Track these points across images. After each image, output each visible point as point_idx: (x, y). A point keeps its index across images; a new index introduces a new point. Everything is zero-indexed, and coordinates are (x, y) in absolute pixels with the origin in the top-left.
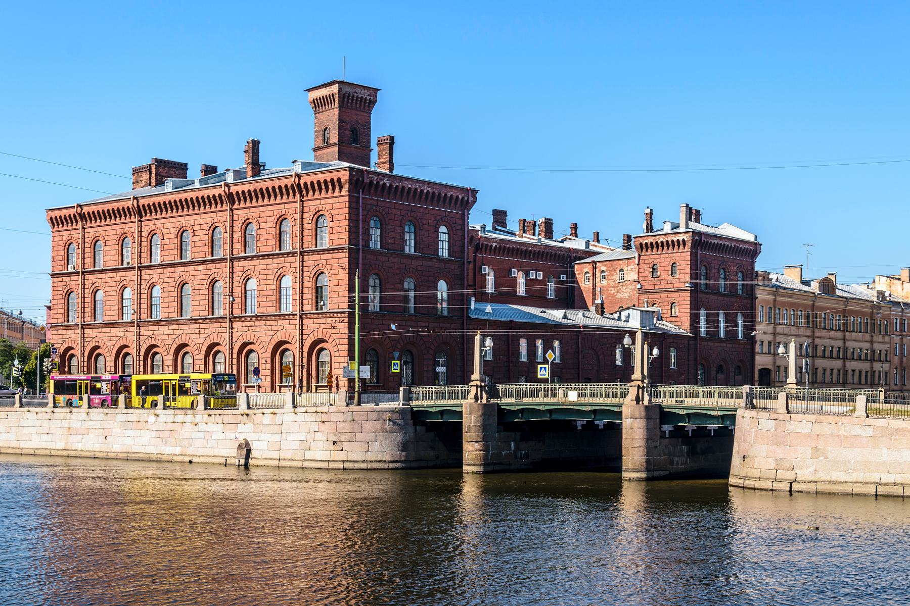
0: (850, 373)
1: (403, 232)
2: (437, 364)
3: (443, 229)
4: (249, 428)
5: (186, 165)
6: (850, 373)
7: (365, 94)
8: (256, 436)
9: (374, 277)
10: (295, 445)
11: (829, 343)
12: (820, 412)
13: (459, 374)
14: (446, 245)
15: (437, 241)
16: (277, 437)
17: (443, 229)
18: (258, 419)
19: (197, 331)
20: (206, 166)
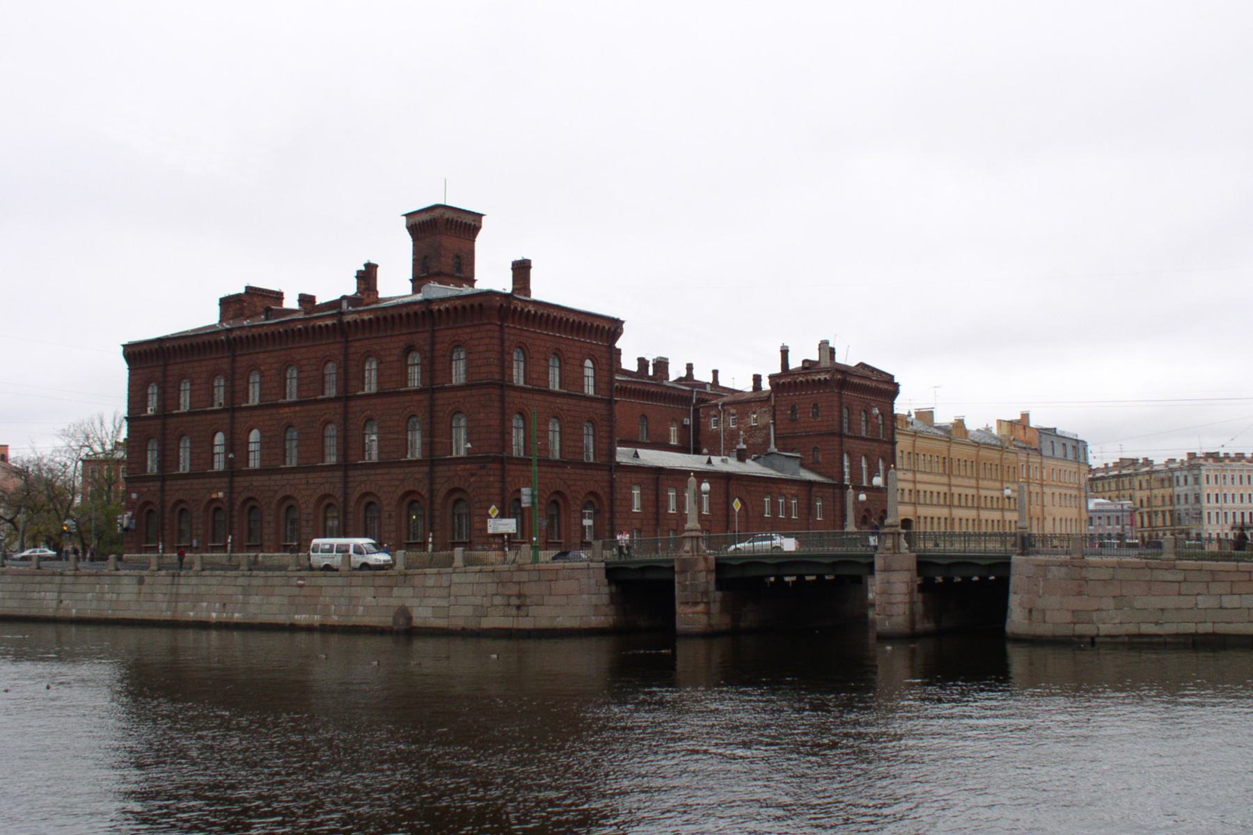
0: (957, 521)
1: (548, 367)
2: (583, 516)
3: (588, 363)
4: (409, 591)
5: (281, 294)
6: (957, 521)
7: (468, 220)
8: (416, 602)
9: (518, 416)
10: (469, 611)
11: (964, 491)
12: (254, 565)
13: (607, 527)
14: (591, 381)
15: (582, 376)
16: (444, 603)
17: (588, 363)
18: (417, 581)
19: (304, 481)
20: (376, 266)
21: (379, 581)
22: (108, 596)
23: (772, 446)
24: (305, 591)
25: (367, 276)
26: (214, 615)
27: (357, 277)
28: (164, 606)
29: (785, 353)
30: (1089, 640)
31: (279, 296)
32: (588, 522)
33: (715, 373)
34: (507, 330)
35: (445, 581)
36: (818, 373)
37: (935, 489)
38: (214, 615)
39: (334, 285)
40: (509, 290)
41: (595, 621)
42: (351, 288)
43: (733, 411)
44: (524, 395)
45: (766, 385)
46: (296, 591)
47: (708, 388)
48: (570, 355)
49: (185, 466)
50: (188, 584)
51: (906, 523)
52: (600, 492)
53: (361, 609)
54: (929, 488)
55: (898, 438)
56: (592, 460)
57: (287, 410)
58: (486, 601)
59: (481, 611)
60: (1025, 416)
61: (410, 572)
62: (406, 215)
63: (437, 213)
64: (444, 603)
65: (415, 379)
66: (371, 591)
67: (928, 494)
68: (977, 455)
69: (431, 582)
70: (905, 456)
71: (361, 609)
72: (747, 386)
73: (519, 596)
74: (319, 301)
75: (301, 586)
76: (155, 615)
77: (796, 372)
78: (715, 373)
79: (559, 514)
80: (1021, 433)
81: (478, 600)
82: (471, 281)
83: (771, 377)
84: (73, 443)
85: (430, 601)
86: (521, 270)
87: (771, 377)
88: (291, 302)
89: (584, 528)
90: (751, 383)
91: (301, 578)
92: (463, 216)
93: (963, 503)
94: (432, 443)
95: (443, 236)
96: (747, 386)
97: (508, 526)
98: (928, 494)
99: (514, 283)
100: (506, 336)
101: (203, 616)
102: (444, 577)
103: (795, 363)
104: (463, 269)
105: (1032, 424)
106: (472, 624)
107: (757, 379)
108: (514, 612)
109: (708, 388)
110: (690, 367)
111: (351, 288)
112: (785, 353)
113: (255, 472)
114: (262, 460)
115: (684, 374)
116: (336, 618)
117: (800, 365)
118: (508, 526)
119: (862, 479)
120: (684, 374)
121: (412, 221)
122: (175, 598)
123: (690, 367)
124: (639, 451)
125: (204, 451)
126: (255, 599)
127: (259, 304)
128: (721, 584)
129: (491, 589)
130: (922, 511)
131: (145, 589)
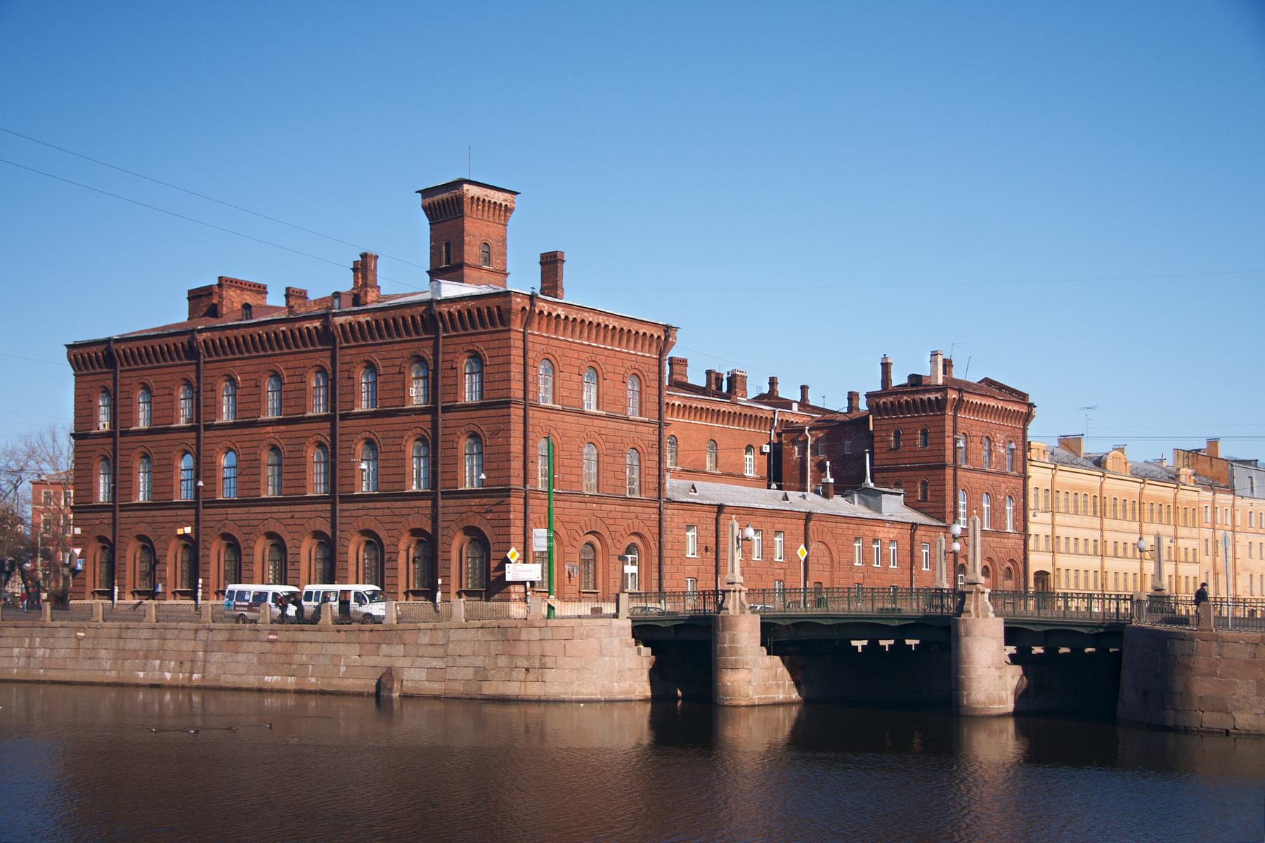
8: (406, 662)
16: (439, 664)
18: (408, 637)
21: (366, 637)
22: (40, 652)
23: (869, 480)
24: (278, 647)
25: (364, 267)
26: (168, 676)
28: (108, 665)
29: (886, 367)
31: (261, 290)
32: (630, 569)
33: (804, 389)
34: (530, 338)
35: (440, 637)
36: (929, 391)
37: (1082, 534)
39: (327, 280)
42: (346, 283)
44: (552, 416)
45: (863, 405)
46: (268, 646)
47: (795, 407)
48: (610, 368)
49: (102, 496)
50: (139, 639)
51: (1042, 576)
52: (645, 532)
53: (343, 669)
54: (1072, 533)
55: (1031, 471)
57: (269, 429)
58: (488, 662)
60: (1213, 443)
61: (401, 626)
62: (68, 346)
64: (439, 664)
65: (416, 394)
66: (356, 648)
67: (1072, 542)
68: (1175, 498)
69: (425, 639)
70: (1041, 493)
71: (343, 669)
72: (841, 405)
74: (313, 296)
76: (97, 677)
77: (901, 389)
78: (804, 389)
79: (595, 560)
80: (1207, 467)
81: (479, 661)
83: (868, 395)
84: (11, 464)
85: (424, 662)
86: (551, 264)
87: (868, 395)
88: (275, 299)
89: (624, 577)
91: (273, 632)
93: (1081, 550)
94: (114, 488)
96: (841, 405)
97: (533, 572)
98: (1072, 542)
99: (543, 281)
100: (530, 345)
101: (154, 677)
102: (441, 633)
105: (1222, 454)
106: (473, 690)
107: (852, 397)
109: (795, 407)
110: (773, 382)
111: (346, 283)
112: (886, 367)
113: (142, 507)
114: (239, 489)
115: (766, 390)
116: (313, 680)
117: (905, 381)
118: (533, 572)
119: (1005, 525)
120: (766, 390)
121: (429, 200)
122: (122, 655)
123: (773, 382)
124: (697, 484)
125: (390, 467)
126: (217, 657)
127: (236, 299)
130: (1064, 561)
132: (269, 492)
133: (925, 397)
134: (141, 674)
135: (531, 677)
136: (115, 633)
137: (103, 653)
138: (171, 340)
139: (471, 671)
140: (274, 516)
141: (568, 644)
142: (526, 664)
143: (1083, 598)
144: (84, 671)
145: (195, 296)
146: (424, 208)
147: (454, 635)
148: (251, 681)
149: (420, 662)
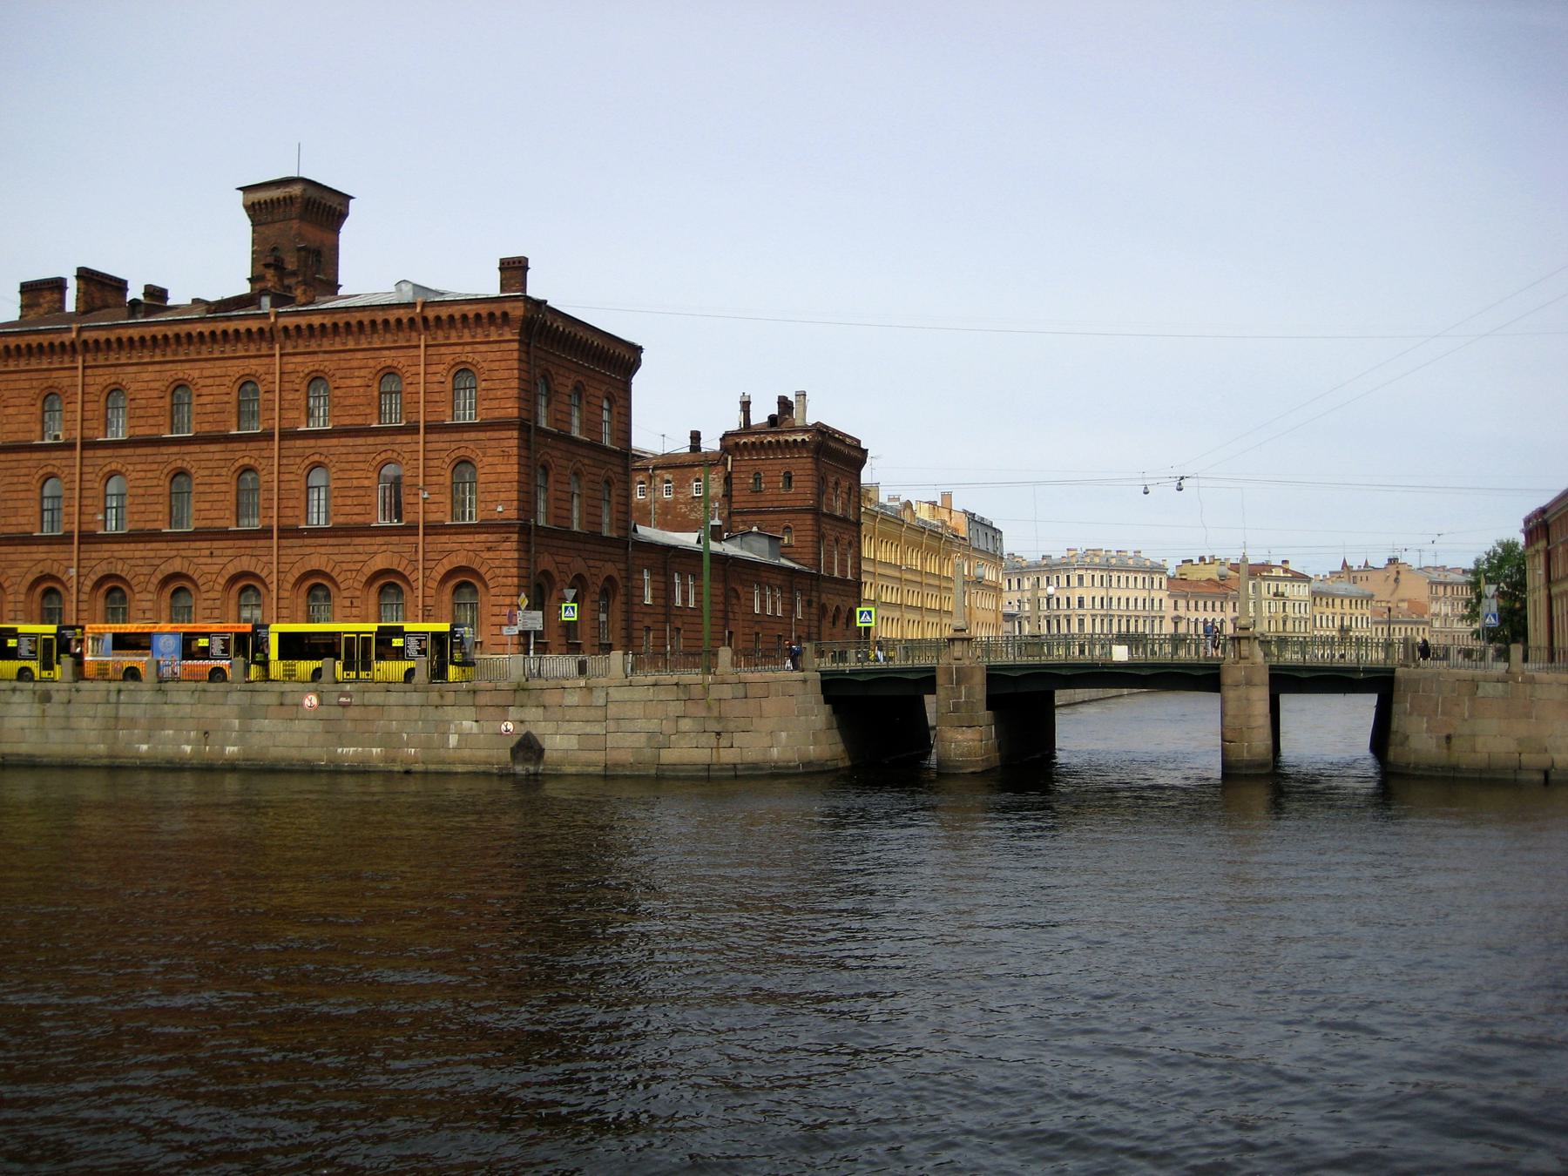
4: (532, 713)
7: (334, 202)
8: (549, 727)
10: (641, 740)
16: (597, 729)
24: (353, 713)
26: (188, 749)
27: (21, 292)
29: (746, 406)
30: (1540, 777)
38: (188, 749)
40: (495, 291)
41: (814, 751)
43: (668, 477)
56: (322, 522)
58: (668, 727)
59: (659, 741)
63: (296, 190)
64: (597, 729)
69: (572, 699)
73: (719, 718)
75: (345, 705)
81: (653, 725)
82: (332, 287)
85: (577, 727)
90: (689, 442)
92: (326, 195)
95: (298, 223)
96: (682, 445)
101: (168, 750)
103: (759, 417)
104: (320, 267)
108: (713, 741)
112: (746, 406)
128: (992, 703)
129: (675, 708)
131: (54, 709)
132: (318, 519)
133: (791, 439)
134: (144, 747)
135: (724, 742)
136: (98, 697)
137: (85, 722)
138: (467, 308)
139: (643, 738)
140: (183, 553)
141: (764, 702)
142: (718, 728)
143: (1323, 644)
144: (56, 744)
145: (30, 290)
146: (247, 207)
147: (615, 694)
148: (317, 753)
149: (566, 727)
